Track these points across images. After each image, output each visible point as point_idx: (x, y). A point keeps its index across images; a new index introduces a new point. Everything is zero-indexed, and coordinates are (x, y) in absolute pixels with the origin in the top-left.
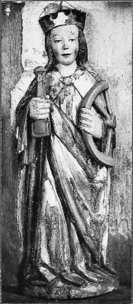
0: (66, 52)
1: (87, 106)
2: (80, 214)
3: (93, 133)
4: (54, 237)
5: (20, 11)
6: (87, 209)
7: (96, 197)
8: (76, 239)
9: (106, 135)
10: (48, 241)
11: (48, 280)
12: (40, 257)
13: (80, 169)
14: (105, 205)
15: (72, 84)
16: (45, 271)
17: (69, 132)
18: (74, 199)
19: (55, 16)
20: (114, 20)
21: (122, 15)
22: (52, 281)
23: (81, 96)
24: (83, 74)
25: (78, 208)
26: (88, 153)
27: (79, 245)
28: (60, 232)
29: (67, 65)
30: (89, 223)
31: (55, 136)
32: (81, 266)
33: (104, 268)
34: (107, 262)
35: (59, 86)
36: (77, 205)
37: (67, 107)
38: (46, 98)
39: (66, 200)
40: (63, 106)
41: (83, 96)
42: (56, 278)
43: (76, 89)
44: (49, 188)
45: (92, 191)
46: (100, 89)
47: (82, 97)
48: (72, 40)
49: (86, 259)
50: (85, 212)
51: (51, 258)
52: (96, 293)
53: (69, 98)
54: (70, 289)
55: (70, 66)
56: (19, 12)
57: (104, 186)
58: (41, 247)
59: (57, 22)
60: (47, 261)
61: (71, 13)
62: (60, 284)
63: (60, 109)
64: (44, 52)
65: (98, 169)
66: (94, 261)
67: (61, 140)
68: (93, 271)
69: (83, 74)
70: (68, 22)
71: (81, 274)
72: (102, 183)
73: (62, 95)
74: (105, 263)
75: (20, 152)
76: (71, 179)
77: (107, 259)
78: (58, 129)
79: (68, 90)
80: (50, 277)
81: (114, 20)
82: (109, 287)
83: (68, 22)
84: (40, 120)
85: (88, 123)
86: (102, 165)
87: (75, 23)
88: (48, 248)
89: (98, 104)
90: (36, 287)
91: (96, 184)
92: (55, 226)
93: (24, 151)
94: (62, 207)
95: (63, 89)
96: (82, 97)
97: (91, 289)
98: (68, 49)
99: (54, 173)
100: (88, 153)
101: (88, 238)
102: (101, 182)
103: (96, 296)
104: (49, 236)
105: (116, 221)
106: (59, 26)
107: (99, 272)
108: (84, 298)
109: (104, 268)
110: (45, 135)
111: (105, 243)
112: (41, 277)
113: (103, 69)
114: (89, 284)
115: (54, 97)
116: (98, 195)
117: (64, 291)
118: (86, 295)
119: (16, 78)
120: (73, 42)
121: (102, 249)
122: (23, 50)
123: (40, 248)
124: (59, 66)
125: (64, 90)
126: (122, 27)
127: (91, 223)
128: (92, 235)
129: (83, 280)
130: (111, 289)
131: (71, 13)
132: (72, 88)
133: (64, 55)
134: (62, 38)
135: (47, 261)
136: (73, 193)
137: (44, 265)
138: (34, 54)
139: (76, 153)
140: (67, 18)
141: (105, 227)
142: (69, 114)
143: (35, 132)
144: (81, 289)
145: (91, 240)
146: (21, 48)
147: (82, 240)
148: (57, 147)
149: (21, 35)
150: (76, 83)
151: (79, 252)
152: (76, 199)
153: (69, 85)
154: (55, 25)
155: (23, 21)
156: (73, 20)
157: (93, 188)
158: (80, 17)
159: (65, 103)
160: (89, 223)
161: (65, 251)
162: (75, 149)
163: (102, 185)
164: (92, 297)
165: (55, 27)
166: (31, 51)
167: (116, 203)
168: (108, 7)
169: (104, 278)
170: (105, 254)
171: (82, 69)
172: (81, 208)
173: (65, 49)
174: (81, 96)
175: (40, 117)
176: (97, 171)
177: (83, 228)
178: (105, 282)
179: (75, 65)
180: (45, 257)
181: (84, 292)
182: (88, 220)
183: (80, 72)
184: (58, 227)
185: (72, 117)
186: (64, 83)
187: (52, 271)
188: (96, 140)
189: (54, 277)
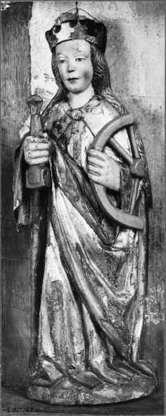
0: (72, 75)
1: (97, 147)
2: (94, 293)
3: (104, 183)
4: (58, 322)
5: (27, 25)
6: (101, 286)
7: (115, 269)
8: (90, 326)
9: (128, 186)
10: (51, 326)
11: (51, 378)
12: (41, 348)
13: (91, 232)
14: (133, 281)
15: (81, 119)
16: (50, 366)
17: (74, 182)
18: (84, 271)
19: (58, 28)
20: (146, 33)
21: (156, 25)
22: (58, 379)
23: (93, 134)
24: (99, 105)
25: (90, 285)
26: (99, 211)
27: (95, 334)
28: (65, 315)
29: (78, 92)
30: (106, 305)
31: (59, 189)
32: (98, 360)
33: (135, 368)
34: (137, 359)
35: (65, 121)
36: (87, 280)
37: (74, 149)
38: (41, 137)
39: (72, 272)
40: (70, 148)
41: (125, 132)
42: (63, 377)
43: (86, 125)
44: (52, 253)
45: (108, 261)
46: (118, 124)
47: (94, 135)
48: (80, 60)
49: (107, 353)
50: (99, 289)
51: (55, 349)
52: (114, 398)
53: (76, 137)
54: (79, 391)
55: (81, 94)
56: (25, 25)
57: (127, 255)
58: (43, 334)
59: (61, 36)
60: (50, 353)
61: (79, 23)
62: (68, 384)
63: (65, 152)
64: (134, 68)
65: (118, 232)
66: (118, 355)
67: (65, 191)
68: (114, 369)
69: (99, 105)
70: (74, 36)
71: (97, 372)
72: (125, 251)
73: (68, 134)
74: (134, 360)
75: (15, 208)
76: (77, 244)
77: (137, 354)
78: (62, 177)
79: (76, 126)
80: (54, 374)
81: (146, 33)
82: (135, 393)
83: (74, 36)
84: (34, 165)
85: (97, 169)
86: (124, 228)
87: (84, 36)
88: (52, 336)
89: (116, 144)
90: (41, 388)
91: (114, 253)
92: (58, 307)
93: (19, 207)
94: (68, 282)
95: (70, 124)
96: (94, 135)
97: (107, 393)
98: (73, 71)
99: (57, 237)
100: (99, 211)
101: (108, 325)
102: (123, 249)
103: (115, 404)
104: (52, 319)
105: (159, 304)
106: (64, 41)
107: (125, 371)
108: (63, 405)
109: (135, 368)
110: (40, 186)
111: (138, 333)
112: (45, 376)
113: (134, 98)
114: (106, 386)
115: (58, 136)
116: (119, 268)
117: (71, 394)
118: (99, 402)
119: (26, 114)
120: (80, 62)
121: (133, 342)
122: (33, 75)
123: (42, 336)
124: (71, 95)
125: (70, 127)
126: (157, 41)
127: (109, 305)
128: (113, 321)
129: (97, 382)
130: (137, 394)
131: (79, 23)
132: (82, 124)
133: (69, 79)
134: (67, 57)
135: (50, 352)
136: (81, 263)
137: (47, 358)
138: (46, 81)
139: (82, 209)
140: (72, 30)
141: (139, 312)
142: (77, 158)
143: (30, 183)
144: (95, 392)
145: (112, 328)
146: (30, 75)
147: (98, 329)
148: (61, 203)
149: (29, 56)
150: (87, 117)
151: (95, 342)
152: (87, 271)
153: (78, 120)
154: (59, 41)
155: (31, 38)
156: (81, 33)
157: (110, 258)
158: (97, 32)
159: (71, 141)
160: (106, 305)
161: (75, 340)
162: (80, 204)
163: (124, 253)
164: (109, 404)
165: (58, 44)
166: (42, 78)
167: (158, 280)
168: (137, 15)
169: (129, 381)
170: (137, 347)
171: (99, 99)
172: (94, 284)
173: (70, 72)
174: (93, 134)
175: (34, 162)
176: (115, 235)
177: (99, 313)
178: (128, 385)
179: (90, 92)
180: (48, 348)
181: (97, 396)
182: (105, 300)
183: (95, 102)
184: (61, 309)
185: (80, 161)
186: (71, 118)
187: (58, 368)
188: (110, 192)
189: (61, 375)
